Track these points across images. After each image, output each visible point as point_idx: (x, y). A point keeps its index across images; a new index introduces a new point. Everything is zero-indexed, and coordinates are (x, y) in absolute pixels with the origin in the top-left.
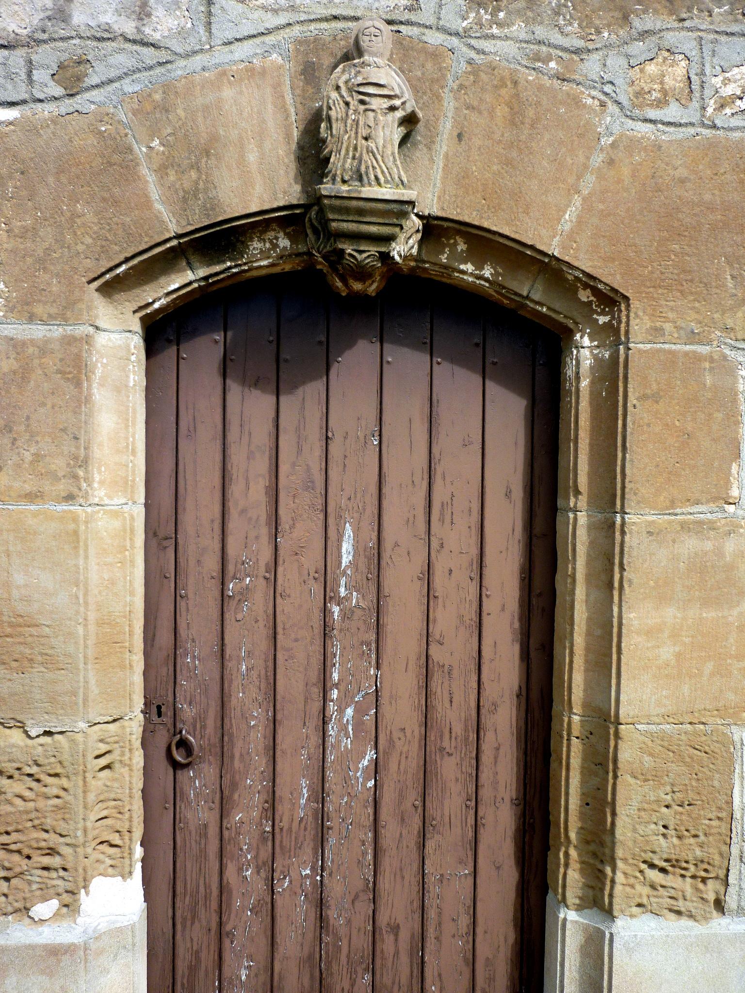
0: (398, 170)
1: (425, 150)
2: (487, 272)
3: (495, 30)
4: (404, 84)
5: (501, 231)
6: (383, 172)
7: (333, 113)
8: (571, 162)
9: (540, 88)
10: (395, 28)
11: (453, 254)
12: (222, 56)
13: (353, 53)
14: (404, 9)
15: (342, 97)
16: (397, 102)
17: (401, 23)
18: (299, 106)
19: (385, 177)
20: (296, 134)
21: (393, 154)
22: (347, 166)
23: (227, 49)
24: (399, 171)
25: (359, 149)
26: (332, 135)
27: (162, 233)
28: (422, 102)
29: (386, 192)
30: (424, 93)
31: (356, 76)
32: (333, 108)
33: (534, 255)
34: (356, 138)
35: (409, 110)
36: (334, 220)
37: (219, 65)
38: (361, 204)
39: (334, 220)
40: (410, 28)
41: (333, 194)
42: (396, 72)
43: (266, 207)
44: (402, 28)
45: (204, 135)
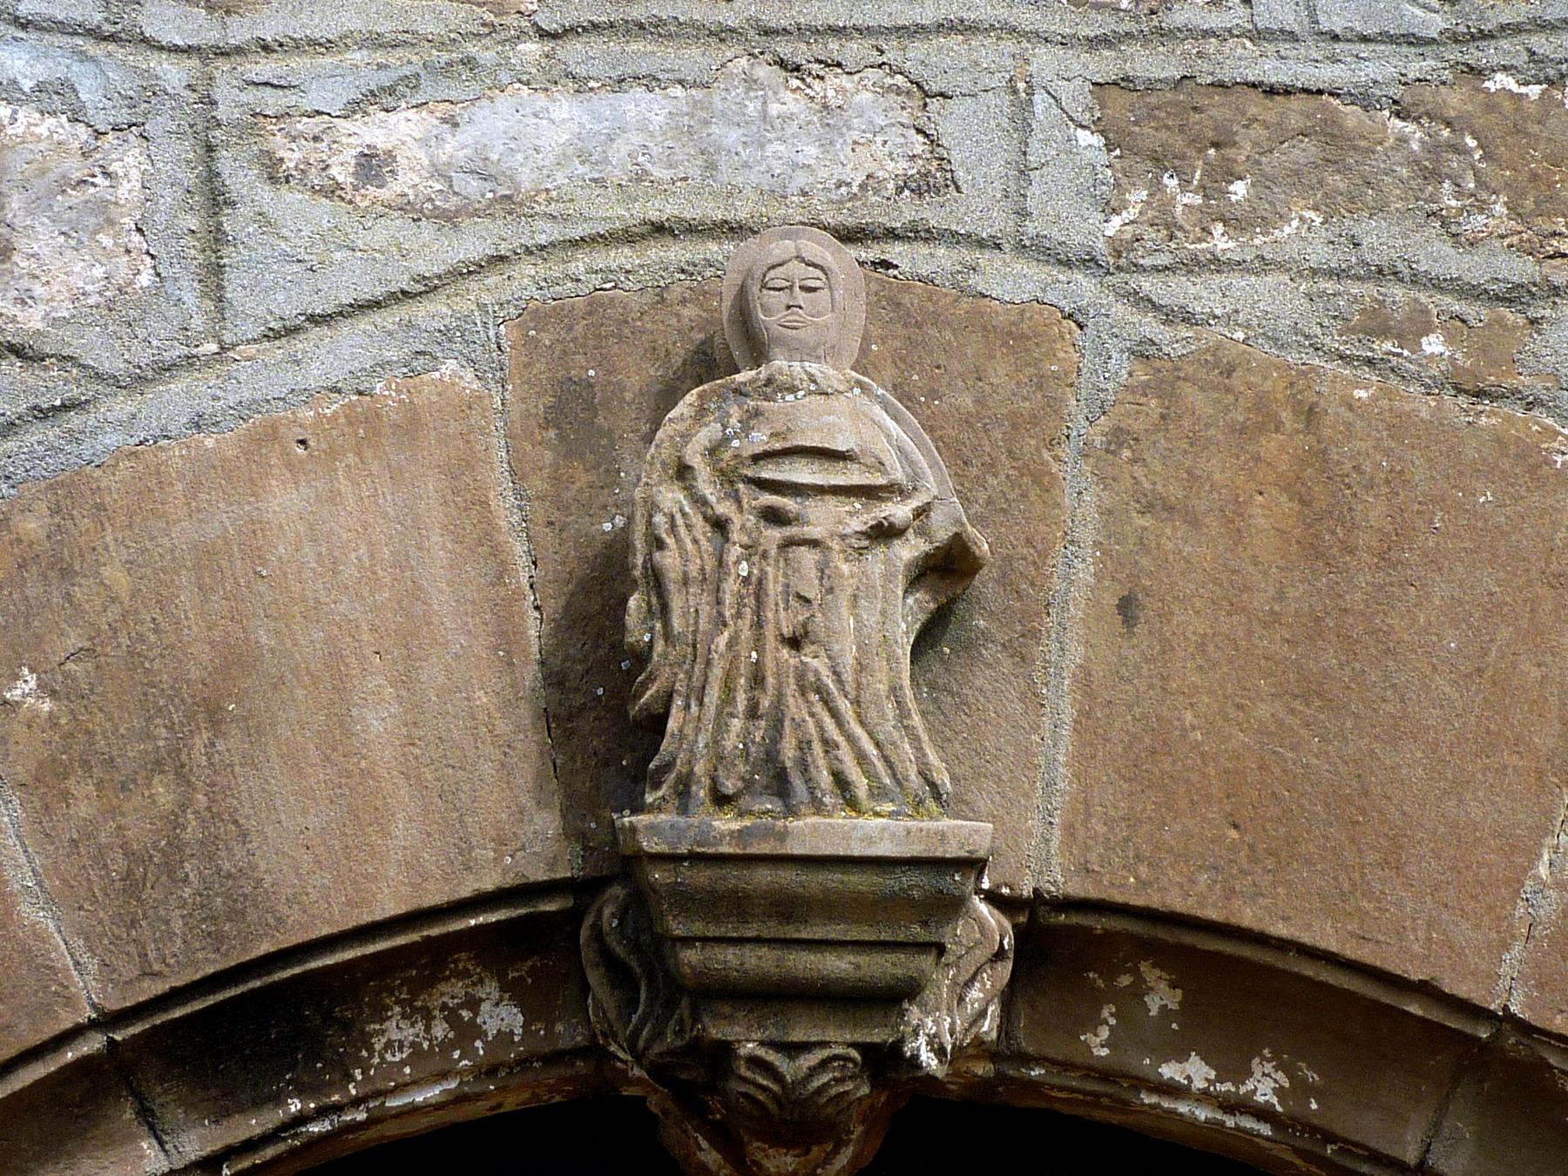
0: (919, 749)
1: (1007, 665)
2: (1264, 1086)
3: (1221, 242)
4: (920, 445)
5: (1306, 938)
6: (861, 758)
7: (669, 560)
8: (1536, 673)
9: (1399, 424)
10: (872, 253)
11: (1130, 1030)
12: (261, 376)
13: (728, 348)
14: (899, 190)
15: (700, 501)
16: (899, 511)
17: (892, 235)
18: (547, 536)
19: (870, 774)
20: (533, 628)
21: (895, 690)
22: (731, 742)
23: (278, 351)
24: (921, 752)
25: (770, 680)
26: (668, 636)
27: (47, 1011)
28: (983, 496)
29: (878, 832)
30: (991, 467)
31: (746, 428)
32: (670, 541)
33: (1436, 1015)
34: (758, 643)
35: (942, 532)
36: (688, 941)
37: (254, 405)
38: (788, 877)
39: (688, 941)
40: (924, 249)
41: (683, 849)
42: (886, 407)
43: (435, 896)
44: (895, 252)
45: (201, 651)
